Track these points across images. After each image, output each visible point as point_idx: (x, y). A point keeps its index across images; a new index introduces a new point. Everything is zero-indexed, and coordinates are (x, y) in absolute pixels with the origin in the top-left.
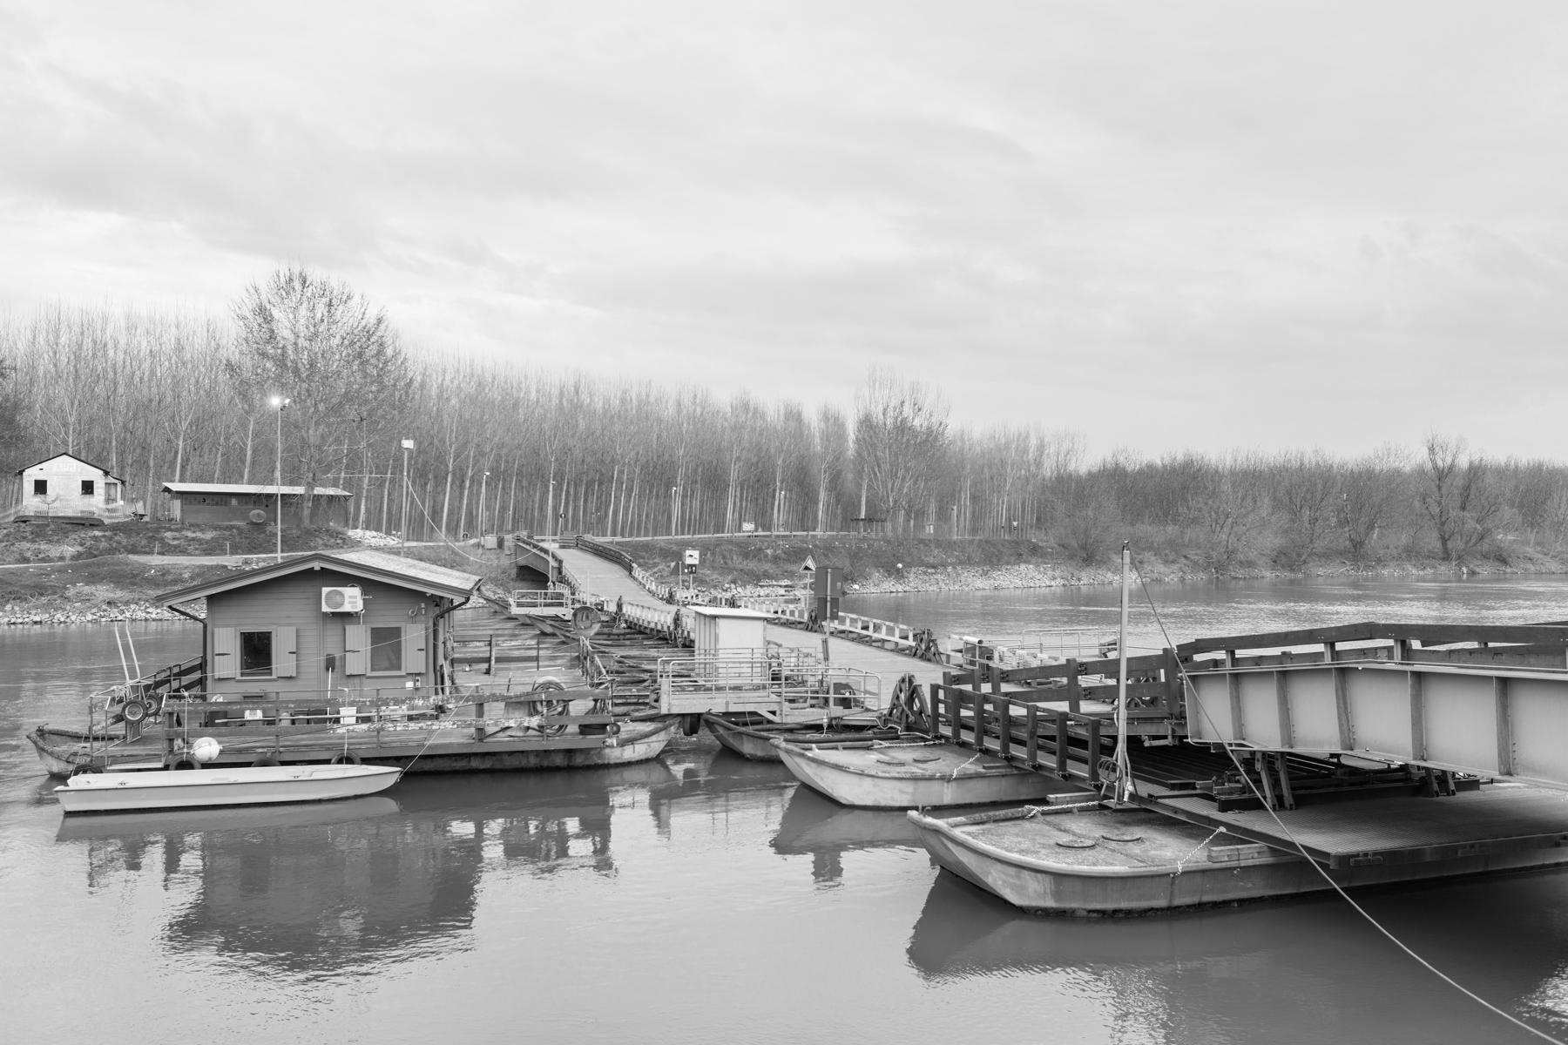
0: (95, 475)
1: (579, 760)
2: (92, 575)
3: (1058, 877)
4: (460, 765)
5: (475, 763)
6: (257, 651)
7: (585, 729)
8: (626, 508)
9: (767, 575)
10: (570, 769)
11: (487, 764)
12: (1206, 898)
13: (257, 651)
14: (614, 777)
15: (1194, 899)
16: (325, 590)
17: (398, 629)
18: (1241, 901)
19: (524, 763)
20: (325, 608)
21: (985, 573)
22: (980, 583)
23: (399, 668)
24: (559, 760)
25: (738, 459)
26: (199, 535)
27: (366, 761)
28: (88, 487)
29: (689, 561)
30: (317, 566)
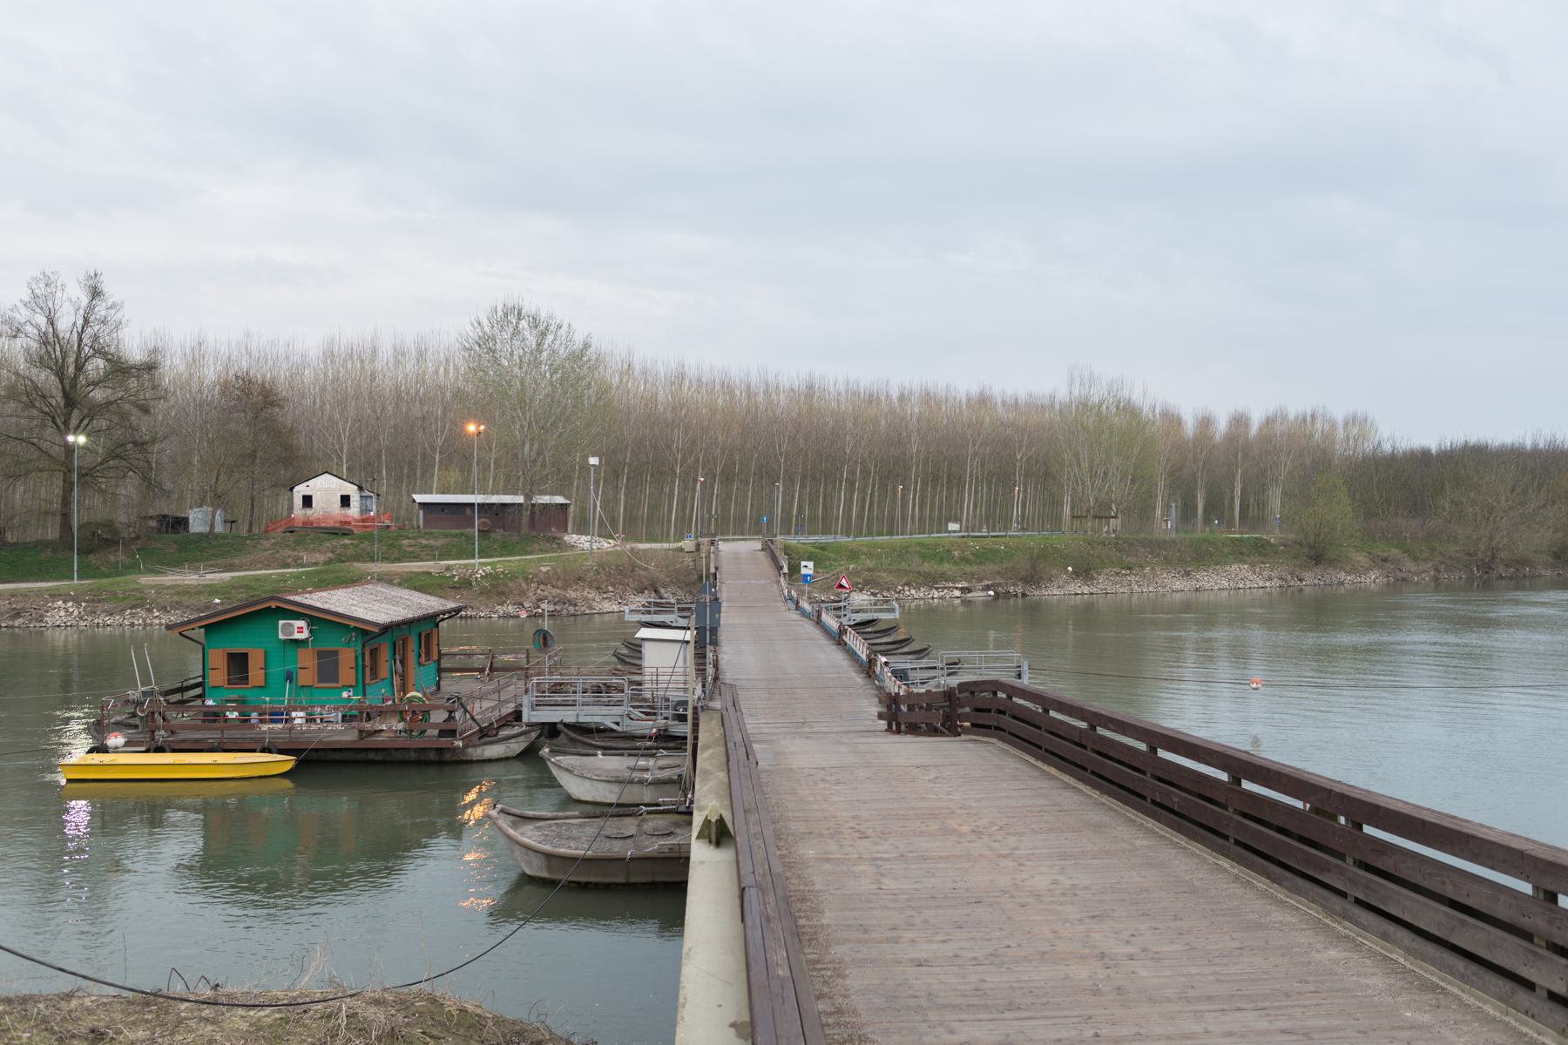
0: (351, 490)
1: (448, 757)
2: (321, 581)
3: (549, 856)
4: (360, 756)
5: (371, 756)
6: (239, 663)
7: (443, 733)
8: (849, 502)
9: (944, 577)
10: (441, 763)
11: (379, 757)
12: (658, 879)
13: (239, 663)
14: (475, 771)
15: (648, 879)
16: (281, 622)
17: (336, 653)
18: (666, 884)
19: (407, 757)
20: (281, 637)
21: (1187, 574)
22: (1178, 585)
23: (337, 681)
24: (432, 756)
25: (975, 454)
26: (432, 542)
27: (280, 752)
28: (345, 501)
29: (804, 571)
30: (273, 605)
